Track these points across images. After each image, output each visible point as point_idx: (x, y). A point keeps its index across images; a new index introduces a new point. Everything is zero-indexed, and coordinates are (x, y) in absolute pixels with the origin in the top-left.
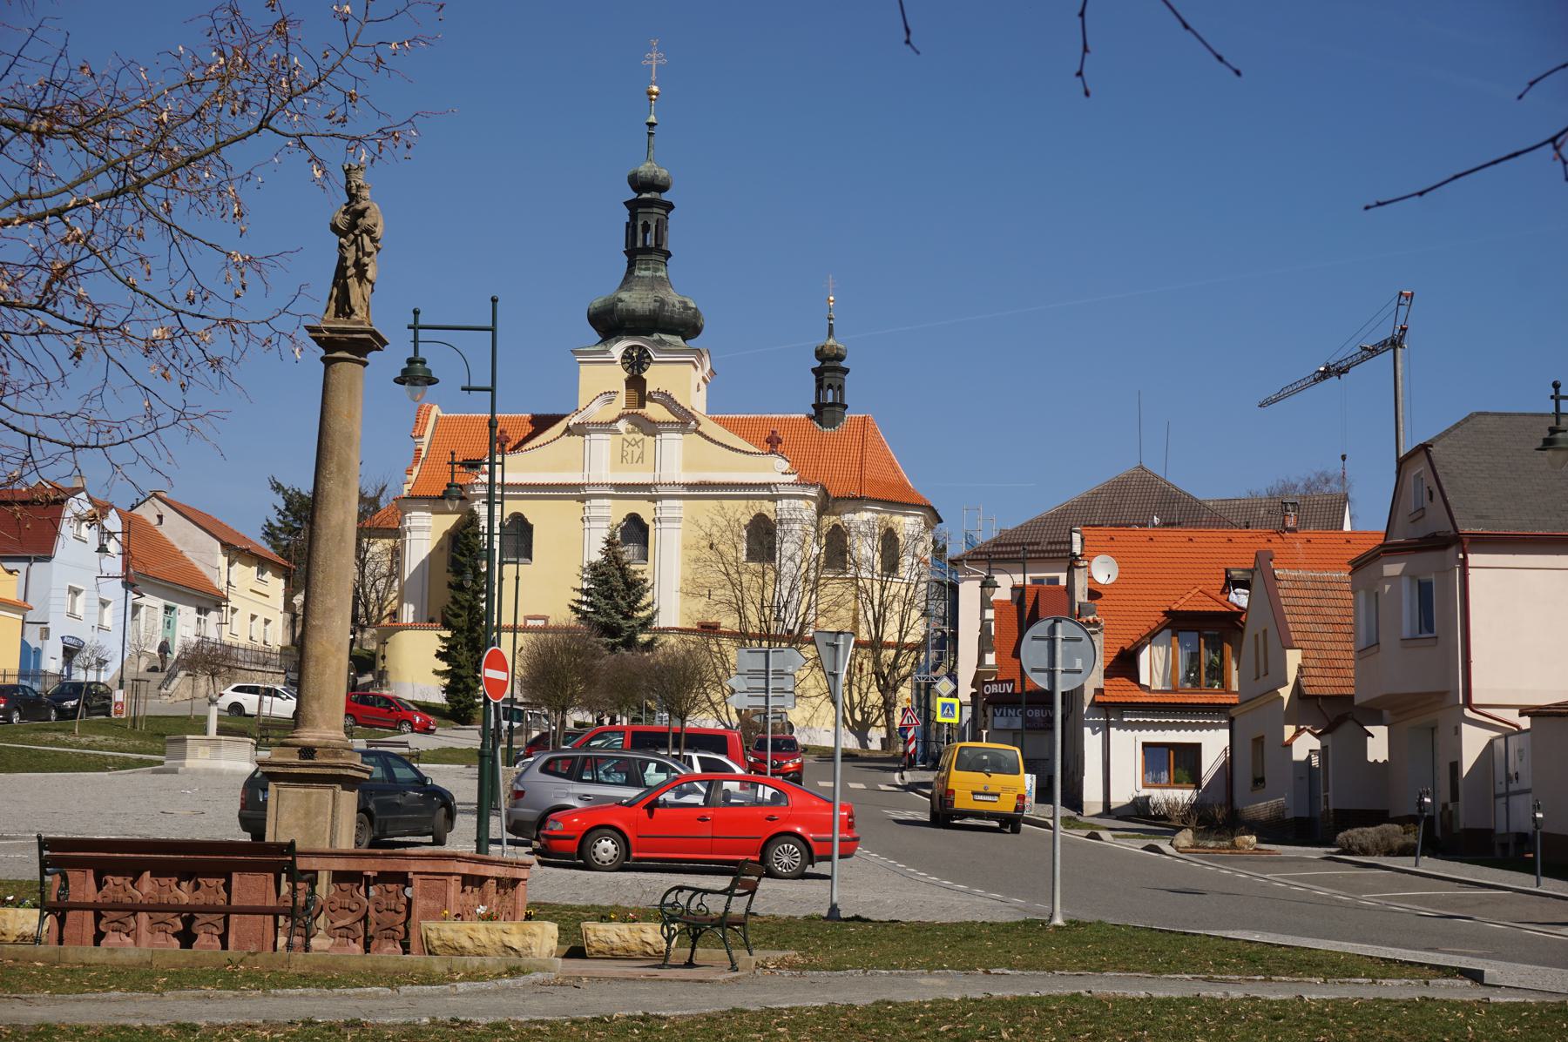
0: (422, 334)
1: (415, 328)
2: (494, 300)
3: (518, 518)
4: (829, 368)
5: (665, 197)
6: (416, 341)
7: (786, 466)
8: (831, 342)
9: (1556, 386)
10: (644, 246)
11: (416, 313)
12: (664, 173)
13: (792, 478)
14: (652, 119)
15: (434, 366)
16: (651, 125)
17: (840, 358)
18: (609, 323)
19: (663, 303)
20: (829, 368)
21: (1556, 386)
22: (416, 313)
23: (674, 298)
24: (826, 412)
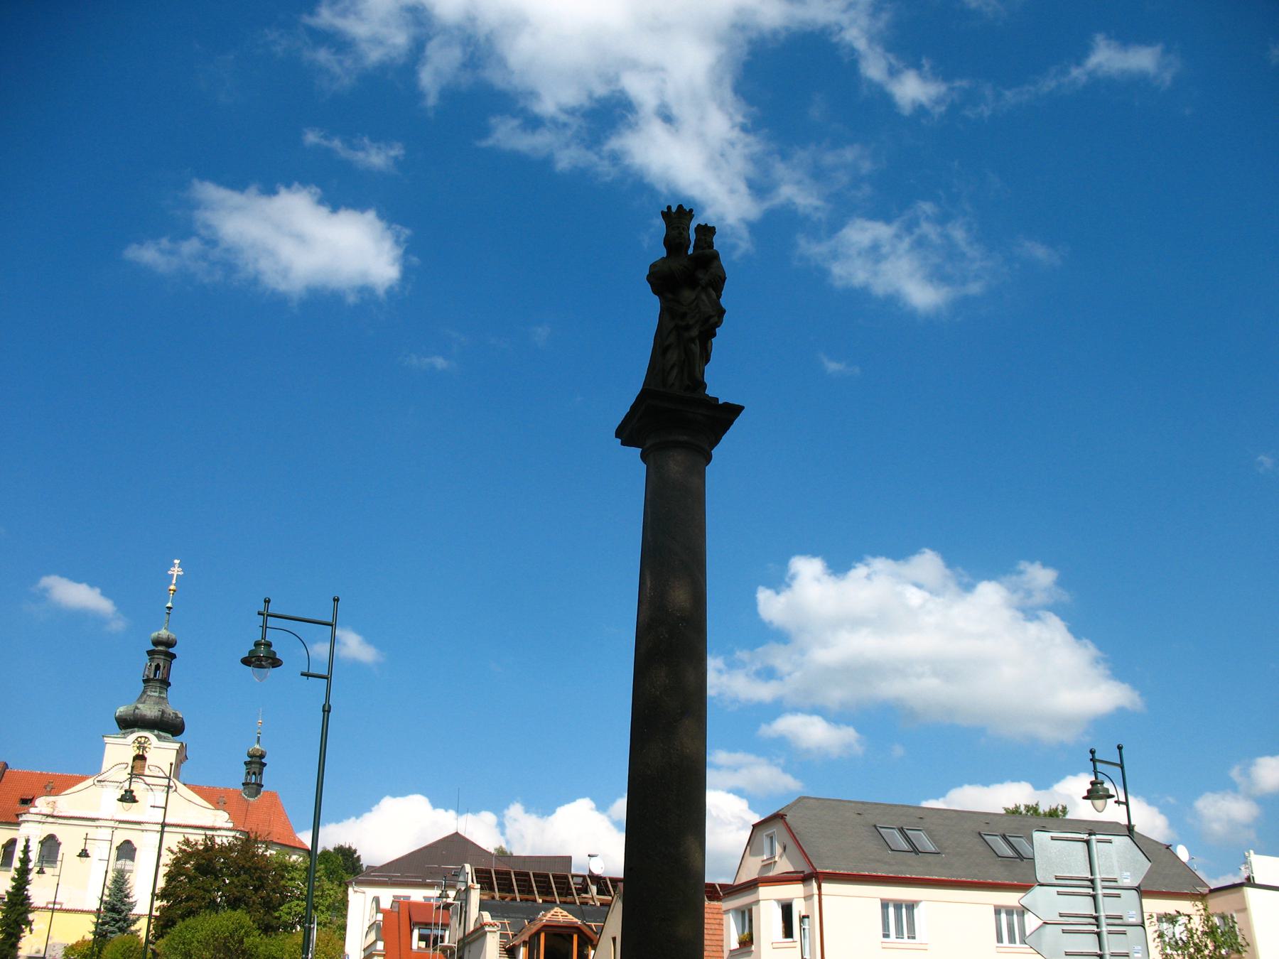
0: (272, 622)
1: (265, 615)
2: (336, 600)
3: (51, 838)
4: (256, 763)
5: (171, 650)
6: (265, 627)
7: (226, 816)
8: (257, 746)
9: (1092, 752)
10: (159, 680)
11: (267, 601)
12: (173, 636)
13: (231, 825)
14: (169, 605)
15: (279, 650)
16: (169, 608)
17: (262, 756)
18: (128, 724)
19: (163, 712)
20: (256, 763)
21: (1092, 752)
22: (267, 601)
23: (170, 710)
24: (254, 787)
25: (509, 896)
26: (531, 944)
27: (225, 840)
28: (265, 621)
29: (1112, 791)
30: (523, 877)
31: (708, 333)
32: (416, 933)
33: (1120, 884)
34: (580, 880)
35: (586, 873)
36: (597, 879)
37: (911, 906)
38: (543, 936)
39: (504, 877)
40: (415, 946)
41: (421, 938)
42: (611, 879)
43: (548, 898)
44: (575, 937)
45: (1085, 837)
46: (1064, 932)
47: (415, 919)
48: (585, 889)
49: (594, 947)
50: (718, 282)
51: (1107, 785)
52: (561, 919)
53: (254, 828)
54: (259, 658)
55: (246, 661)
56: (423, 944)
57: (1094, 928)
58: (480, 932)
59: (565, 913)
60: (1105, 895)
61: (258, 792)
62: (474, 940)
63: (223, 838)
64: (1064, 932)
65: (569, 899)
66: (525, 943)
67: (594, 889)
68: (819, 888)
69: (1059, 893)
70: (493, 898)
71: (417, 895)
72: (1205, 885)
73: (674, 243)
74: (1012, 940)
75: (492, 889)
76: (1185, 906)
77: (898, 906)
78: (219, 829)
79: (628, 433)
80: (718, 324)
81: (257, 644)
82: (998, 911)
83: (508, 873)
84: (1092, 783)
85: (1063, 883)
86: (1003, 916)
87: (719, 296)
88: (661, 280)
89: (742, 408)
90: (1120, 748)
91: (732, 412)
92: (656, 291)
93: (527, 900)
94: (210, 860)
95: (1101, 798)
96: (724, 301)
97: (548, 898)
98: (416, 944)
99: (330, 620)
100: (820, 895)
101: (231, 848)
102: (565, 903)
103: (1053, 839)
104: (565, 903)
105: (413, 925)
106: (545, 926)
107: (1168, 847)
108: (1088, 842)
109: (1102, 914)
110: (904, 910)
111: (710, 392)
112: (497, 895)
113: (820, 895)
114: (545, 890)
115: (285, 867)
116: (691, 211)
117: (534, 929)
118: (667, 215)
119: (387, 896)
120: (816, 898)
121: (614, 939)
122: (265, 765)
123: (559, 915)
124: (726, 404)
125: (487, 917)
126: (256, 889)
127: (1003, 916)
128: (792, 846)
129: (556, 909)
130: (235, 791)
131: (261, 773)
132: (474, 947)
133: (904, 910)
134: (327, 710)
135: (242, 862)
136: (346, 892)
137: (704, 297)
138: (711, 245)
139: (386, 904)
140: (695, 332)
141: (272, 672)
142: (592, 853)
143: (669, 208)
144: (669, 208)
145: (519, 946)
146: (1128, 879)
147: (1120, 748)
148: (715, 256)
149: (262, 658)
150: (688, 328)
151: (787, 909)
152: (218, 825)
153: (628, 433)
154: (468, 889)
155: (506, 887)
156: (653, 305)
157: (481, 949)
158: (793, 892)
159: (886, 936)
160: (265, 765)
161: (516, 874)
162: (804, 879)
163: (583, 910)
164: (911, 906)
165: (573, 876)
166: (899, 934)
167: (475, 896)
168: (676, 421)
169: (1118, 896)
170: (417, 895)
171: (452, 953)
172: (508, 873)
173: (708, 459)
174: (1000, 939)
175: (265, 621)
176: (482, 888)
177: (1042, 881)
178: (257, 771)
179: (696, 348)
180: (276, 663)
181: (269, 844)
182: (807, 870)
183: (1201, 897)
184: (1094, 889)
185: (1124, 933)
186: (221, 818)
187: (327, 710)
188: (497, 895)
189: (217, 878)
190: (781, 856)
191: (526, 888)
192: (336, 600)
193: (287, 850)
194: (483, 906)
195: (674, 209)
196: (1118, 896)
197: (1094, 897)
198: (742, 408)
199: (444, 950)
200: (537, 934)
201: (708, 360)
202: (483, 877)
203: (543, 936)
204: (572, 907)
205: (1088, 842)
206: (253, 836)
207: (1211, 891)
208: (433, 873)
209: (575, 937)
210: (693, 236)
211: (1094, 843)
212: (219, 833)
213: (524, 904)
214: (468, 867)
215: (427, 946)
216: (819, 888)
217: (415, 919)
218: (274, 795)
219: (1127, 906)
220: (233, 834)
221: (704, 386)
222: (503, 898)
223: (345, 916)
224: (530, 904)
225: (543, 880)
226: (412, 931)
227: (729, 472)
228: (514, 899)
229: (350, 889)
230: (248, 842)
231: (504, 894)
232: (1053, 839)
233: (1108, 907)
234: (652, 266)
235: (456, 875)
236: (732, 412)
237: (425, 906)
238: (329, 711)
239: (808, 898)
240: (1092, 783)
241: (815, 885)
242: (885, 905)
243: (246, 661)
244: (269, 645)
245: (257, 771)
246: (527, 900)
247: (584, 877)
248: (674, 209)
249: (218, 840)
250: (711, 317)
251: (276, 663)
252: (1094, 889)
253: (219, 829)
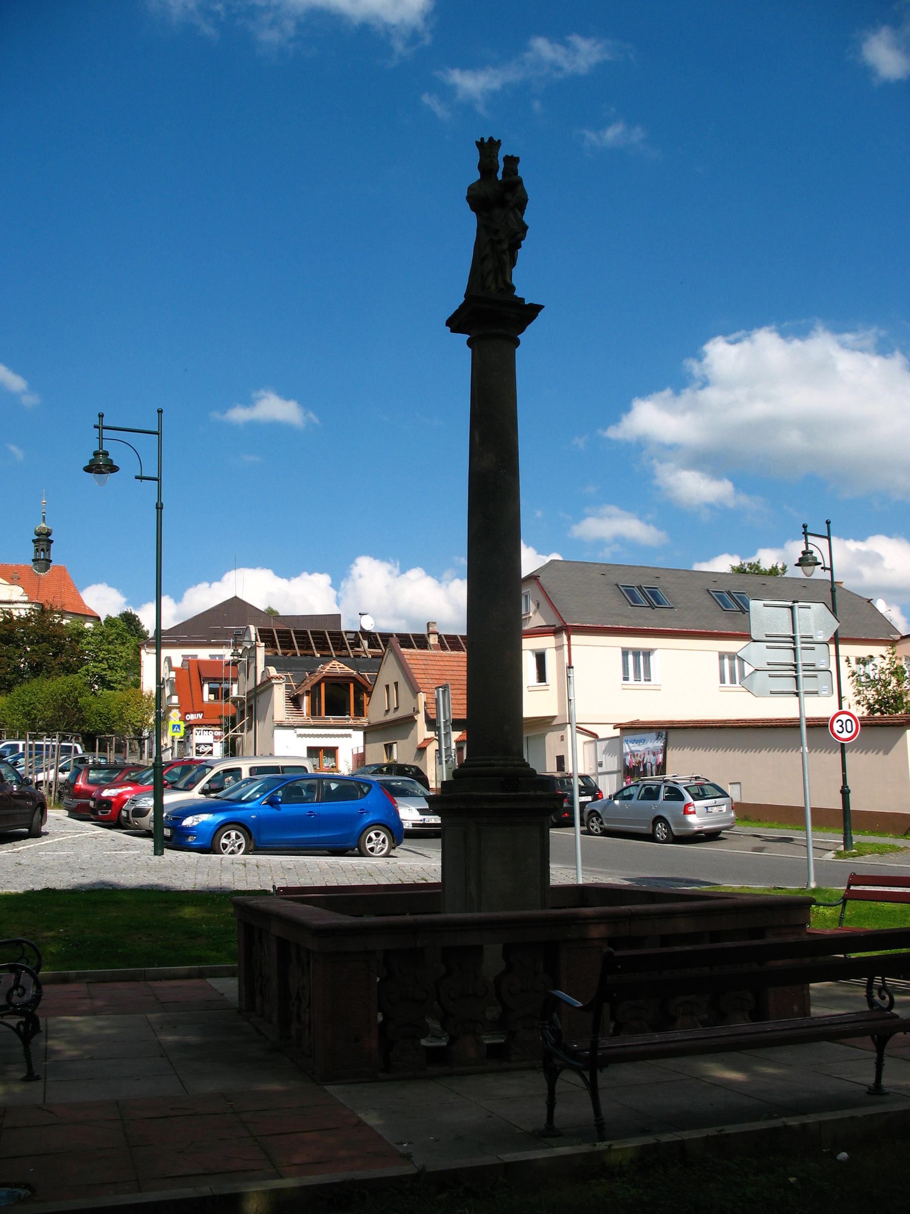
2: (160, 412)
4: (43, 540)
6: (101, 438)
7: (20, 590)
8: (44, 525)
9: (805, 527)
11: (101, 416)
13: (26, 598)
17: (49, 534)
20: (43, 540)
21: (805, 527)
22: (101, 416)
25: (290, 652)
26: (314, 693)
27: (23, 613)
28: (101, 434)
29: (819, 560)
30: (302, 636)
31: (516, 245)
32: (206, 687)
33: (815, 640)
34: (352, 636)
35: (358, 629)
36: (367, 635)
37: (648, 653)
38: (323, 685)
39: (285, 636)
40: (206, 699)
41: (211, 691)
42: (381, 635)
43: (326, 653)
44: (352, 685)
45: (790, 604)
46: (770, 676)
47: (204, 675)
48: (356, 644)
49: (370, 694)
50: (522, 204)
51: (816, 554)
52: (338, 670)
53: (50, 600)
54: (99, 466)
55: (88, 469)
56: (212, 697)
57: (793, 673)
58: (267, 685)
59: (342, 665)
60: (803, 649)
61: (48, 568)
62: (263, 692)
63: (20, 611)
64: (770, 676)
65: (344, 652)
66: (307, 693)
67: (366, 643)
68: (569, 639)
69: (768, 647)
70: (276, 654)
71: (204, 654)
72: (898, 633)
73: (487, 168)
74: (733, 681)
75: (275, 647)
76: (882, 650)
77: (636, 653)
78: (16, 602)
79: (456, 323)
80: (523, 239)
81: (96, 454)
82: (722, 656)
83: (288, 632)
84: (803, 553)
85: (771, 640)
86: (726, 661)
87: (523, 214)
88: (478, 200)
89: (539, 308)
90: (828, 523)
91: (534, 310)
92: (473, 209)
93: (306, 655)
94: (12, 631)
95: (810, 565)
96: (526, 218)
97: (326, 653)
98: (207, 696)
99: (156, 430)
100: (569, 645)
101: (28, 619)
102: (339, 656)
103: (765, 606)
104: (339, 656)
105: (203, 680)
106: (325, 677)
107: (869, 601)
108: (792, 608)
109: (800, 662)
110: (641, 657)
111: (518, 293)
112: (280, 652)
113: (569, 645)
114: (322, 645)
115: (81, 634)
116: (499, 141)
117: (316, 680)
118: (480, 145)
119: (176, 656)
120: (566, 648)
121: (387, 687)
122: (52, 542)
123: (336, 667)
124: (531, 304)
125: (273, 671)
126: (55, 655)
127: (726, 661)
128: (544, 604)
129: (334, 662)
130: (26, 567)
131: (49, 550)
132: (261, 698)
133: (641, 657)
134: (159, 507)
135: (40, 632)
136: (139, 654)
137: (511, 216)
138: (516, 173)
139: (177, 663)
140: (505, 246)
141: (111, 476)
142: (362, 612)
143: (482, 139)
144: (482, 139)
145: (302, 695)
146: (822, 636)
147: (828, 523)
148: (520, 182)
149: (100, 465)
150: (500, 242)
151: (541, 658)
152: (14, 599)
153: (456, 323)
154: (254, 648)
155: (287, 644)
156: (471, 220)
157: (269, 699)
158: (546, 643)
159: (626, 679)
160: (52, 542)
161: (295, 632)
162: (556, 632)
163: (356, 662)
164: (648, 653)
165: (346, 632)
166: (637, 678)
167: (261, 653)
168: (492, 318)
169: (813, 649)
170: (204, 654)
171: (243, 703)
172: (288, 632)
173: (517, 343)
174: (722, 681)
175: (101, 434)
176: (266, 647)
177: (756, 639)
178: (45, 547)
179: (506, 258)
180: (114, 469)
181: (63, 614)
182: (558, 624)
183: (893, 643)
184: (794, 643)
185: (815, 676)
186: (16, 593)
187: (159, 507)
188: (280, 652)
189: (18, 647)
190: (535, 613)
191: (304, 644)
192: (160, 412)
193: (81, 618)
194: (268, 662)
195: (486, 140)
196: (813, 649)
197: (794, 650)
198: (542, 307)
199: (235, 701)
200: (318, 684)
201: (514, 265)
202: (266, 636)
203: (323, 685)
204: (347, 659)
205: (792, 608)
206: (48, 607)
207: (903, 638)
208: (216, 634)
209: (352, 685)
210: (501, 165)
211: (796, 609)
212: (16, 606)
213: (304, 659)
214: (253, 629)
215: (216, 698)
216: (569, 639)
217: (204, 675)
218: (63, 570)
219: (823, 657)
220: (29, 606)
221: (513, 288)
222: (285, 654)
223: (139, 674)
224: (309, 658)
225: (320, 638)
226: (202, 686)
227: (532, 351)
228: (295, 655)
229: (143, 652)
230: (43, 611)
231: (286, 651)
232: (765, 606)
233: (805, 657)
234: (470, 189)
235: (244, 635)
236: (534, 310)
237: (213, 663)
238: (162, 508)
239: (559, 648)
240: (803, 553)
241: (565, 637)
242: (625, 653)
243: (88, 469)
244: (106, 454)
245: (45, 547)
246: (306, 655)
247: (356, 633)
248: (486, 140)
249: (16, 613)
250: (517, 233)
251: (114, 469)
252: (794, 643)
253: (16, 602)
